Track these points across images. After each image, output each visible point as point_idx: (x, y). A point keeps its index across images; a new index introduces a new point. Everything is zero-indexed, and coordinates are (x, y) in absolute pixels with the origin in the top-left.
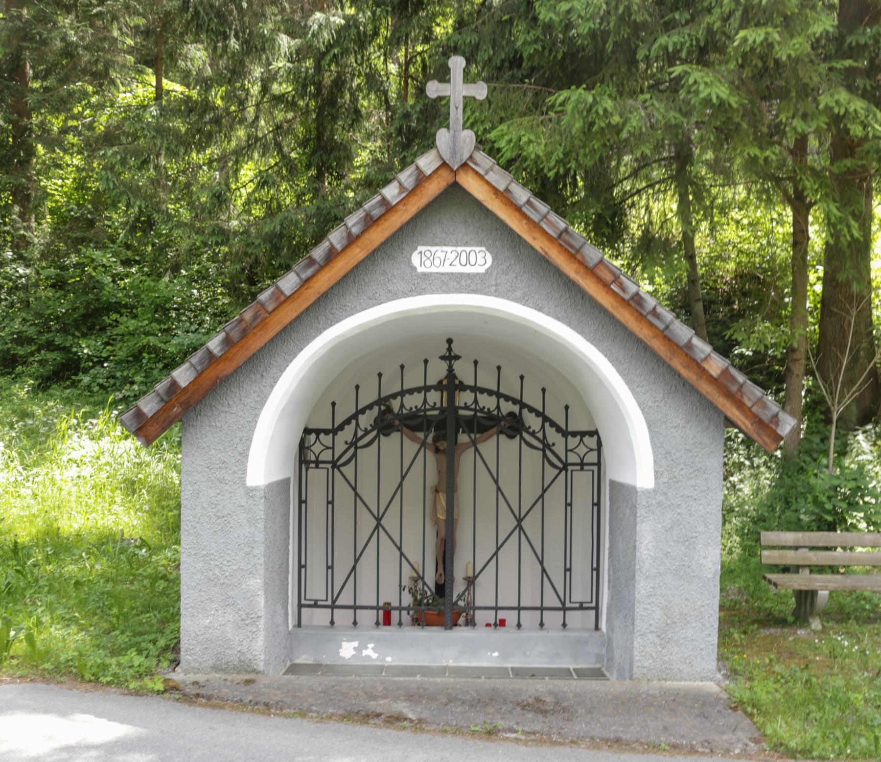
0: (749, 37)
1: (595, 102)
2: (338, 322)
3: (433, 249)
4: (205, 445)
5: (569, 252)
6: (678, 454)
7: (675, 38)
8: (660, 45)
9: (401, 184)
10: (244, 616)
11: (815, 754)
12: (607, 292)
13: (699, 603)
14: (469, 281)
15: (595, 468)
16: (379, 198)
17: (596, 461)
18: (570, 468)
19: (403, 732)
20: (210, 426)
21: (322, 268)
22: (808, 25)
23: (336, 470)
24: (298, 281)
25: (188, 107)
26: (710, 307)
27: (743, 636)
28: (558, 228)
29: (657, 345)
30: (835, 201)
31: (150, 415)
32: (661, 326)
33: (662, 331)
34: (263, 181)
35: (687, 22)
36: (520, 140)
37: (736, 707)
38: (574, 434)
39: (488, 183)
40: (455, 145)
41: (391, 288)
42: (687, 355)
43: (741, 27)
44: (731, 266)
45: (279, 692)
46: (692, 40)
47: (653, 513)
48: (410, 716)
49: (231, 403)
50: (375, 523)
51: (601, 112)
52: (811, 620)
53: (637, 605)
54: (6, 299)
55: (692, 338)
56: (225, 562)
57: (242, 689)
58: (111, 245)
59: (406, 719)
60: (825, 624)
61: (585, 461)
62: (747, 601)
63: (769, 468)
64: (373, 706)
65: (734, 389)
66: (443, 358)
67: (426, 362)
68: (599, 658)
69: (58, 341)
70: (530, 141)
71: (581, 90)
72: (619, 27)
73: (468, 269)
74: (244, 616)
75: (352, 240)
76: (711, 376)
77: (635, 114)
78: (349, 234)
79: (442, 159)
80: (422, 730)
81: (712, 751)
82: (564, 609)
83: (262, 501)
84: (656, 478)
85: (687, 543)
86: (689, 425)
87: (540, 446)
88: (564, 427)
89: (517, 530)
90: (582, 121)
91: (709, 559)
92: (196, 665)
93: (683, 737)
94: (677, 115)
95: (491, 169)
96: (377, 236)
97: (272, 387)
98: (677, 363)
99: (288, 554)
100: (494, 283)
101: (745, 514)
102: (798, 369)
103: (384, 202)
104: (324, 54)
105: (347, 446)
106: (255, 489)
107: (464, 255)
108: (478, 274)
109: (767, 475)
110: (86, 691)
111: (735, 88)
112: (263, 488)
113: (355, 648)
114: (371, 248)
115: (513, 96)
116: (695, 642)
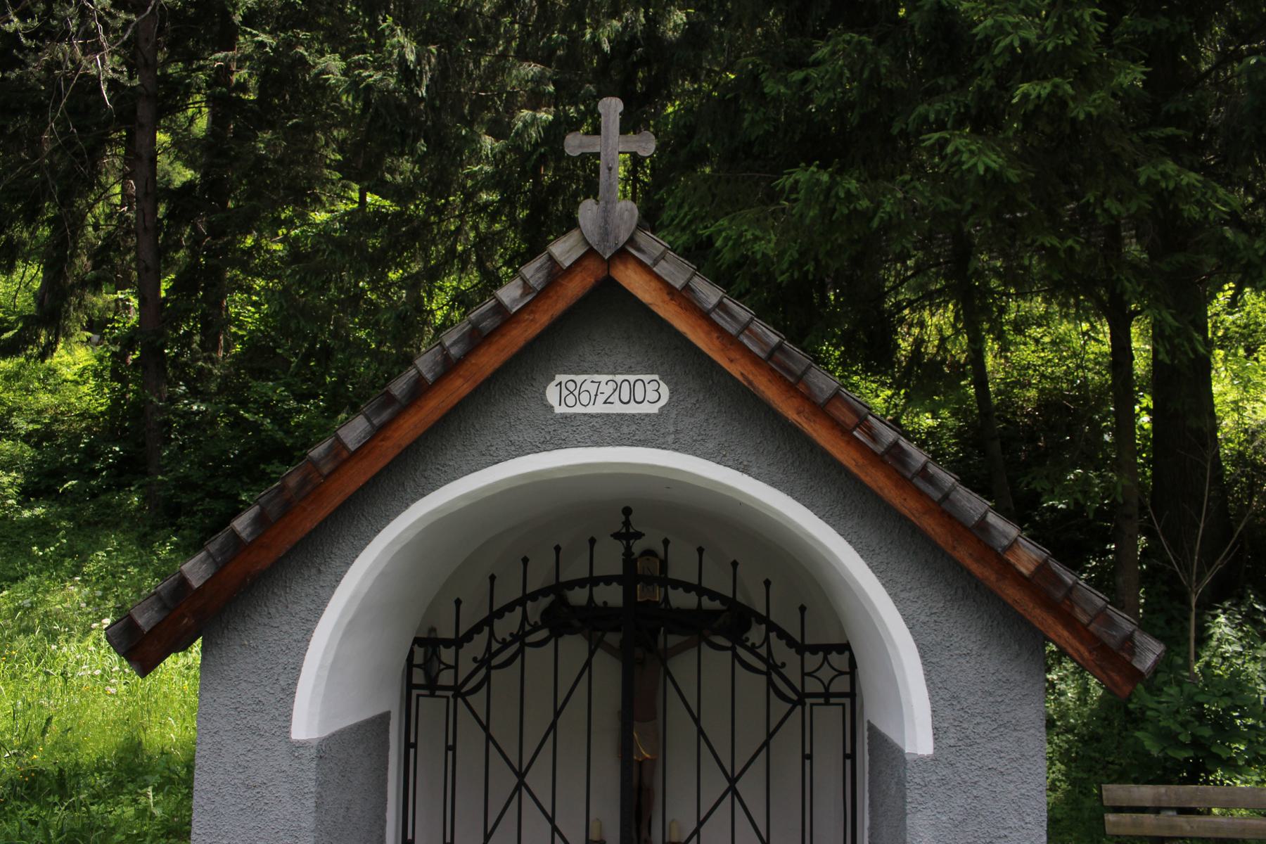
0: (1032, 91)
1: (833, 184)
2: (433, 490)
3: (579, 379)
4: (232, 674)
5: (786, 380)
6: (971, 700)
7: (938, 106)
9: (525, 282)
12: (848, 443)
14: (634, 427)
15: (847, 701)
17: (848, 689)
18: (808, 701)
23: (460, 700)
24: (369, 428)
28: (767, 344)
29: (930, 524)
30: (1168, 307)
31: (147, 630)
32: (937, 495)
33: (939, 503)
35: (954, 89)
36: (741, 235)
38: (814, 649)
39: (658, 277)
40: (606, 222)
41: (514, 438)
42: (979, 541)
44: (1032, 393)
46: (959, 108)
47: (932, 796)
49: (273, 611)
51: (842, 195)
55: (986, 513)
58: (283, 376)
65: (1059, 594)
66: (617, 536)
67: (592, 541)
71: (813, 169)
73: (632, 409)
75: (449, 367)
76: (1021, 574)
77: (889, 196)
78: (446, 357)
79: (587, 243)
83: (313, 765)
86: (987, 652)
87: (762, 667)
89: (729, 796)
90: (817, 207)
95: (663, 257)
96: (489, 360)
97: (334, 588)
98: (963, 554)
99: (383, 828)
100: (672, 429)
101: (1070, 730)
103: (500, 307)
104: (531, 153)
105: (476, 665)
106: (302, 745)
107: (626, 386)
108: (647, 415)
112: (315, 743)
114: (480, 378)
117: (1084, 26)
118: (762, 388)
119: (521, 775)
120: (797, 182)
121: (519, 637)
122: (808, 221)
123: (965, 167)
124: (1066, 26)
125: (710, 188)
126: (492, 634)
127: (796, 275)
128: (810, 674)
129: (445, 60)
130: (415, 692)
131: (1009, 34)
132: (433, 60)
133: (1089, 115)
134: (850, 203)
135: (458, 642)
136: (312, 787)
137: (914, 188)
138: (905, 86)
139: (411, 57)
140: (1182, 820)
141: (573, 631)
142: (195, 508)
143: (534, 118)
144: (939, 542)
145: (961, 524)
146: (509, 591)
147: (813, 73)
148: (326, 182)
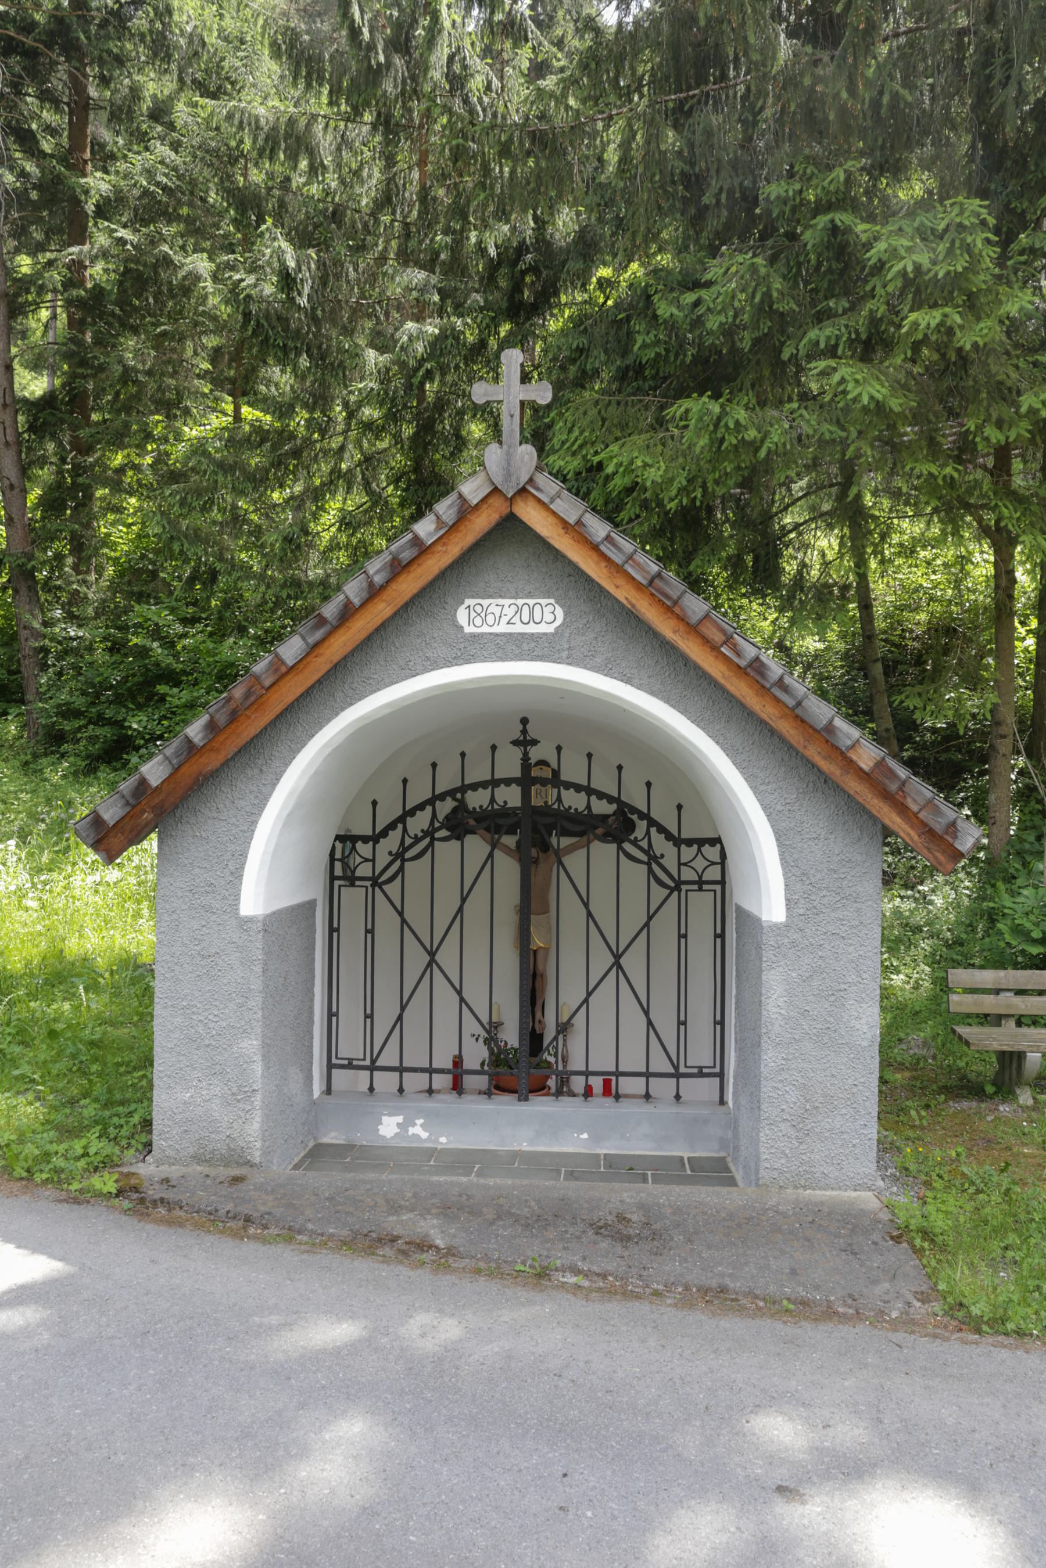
0: (920, 321)
1: (724, 413)
3: (485, 602)
6: (819, 876)
7: (828, 332)
8: (810, 341)
10: (235, 1090)
11: (1010, 1326)
13: (850, 1081)
14: (533, 644)
15: (718, 888)
16: (410, 536)
17: (719, 878)
18: (684, 887)
19: (420, 1271)
20: (194, 836)
21: (335, 629)
22: (1000, 303)
24: (304, 646)
25: (260, 436)
26: (895, 668)
27: (923, 1113)
28: (648, 572)
29: (786, 728)
31: (112, 823)
32: (791, 703)
33: (793, 709)
34: (347, 522)
35: (845, 311)
36: (632, 462)
37: (900, 1236)
38: (689, 842)
39: (554, 513)
40: (509, 464)
43: (911, 310)
44: (923, 617)
45: (271, 1198)
47: (784, 956)
48: (439, 1242)
49: (221, 806)
50: (428, 958)
51: (731, 425)
52: (1018, 1092)
53: (764, 1082)
54: (54, 665)
56: (211, 1017)
57: (223, 1193)
59: (430, 1247)
60: (1039, 1097)
61: (704, 878)
62: (934, 1058)
63: (968, 874)
64: (393, 1224)
65: (893, 787)
66: (515, 743)
67: (494, 748)
68: (723, 1143)
69: (109, 714)
70: (646, 465)
71: (705, 399)
72: (758, 320)
73: (532, 629)
74: (235, 1090)
75: (374, 592)
76: (861, 769)
78: (371, 584)
80: (448, 1268)
81: (858, 1313)
82: (677, 1075)
83: (260, 936)
84: (788, 909)
85: (833, 998)
87: (644, 858)
88: (675, 832)
91: (863, 1021)
92: (172, 1153)
93: (817, 1287)
94: (833, 428)
95: (558, 495)
96: (408, 586)
98: (814, 752)
99: (312, 1000)
100: (566, 646)
102: (1004, 746)
103: (416, 541)
104: (416, 370)
106: (250, 920)
107: (526, 609)
109: (967, 883)
110: (11, 1194)
111: (901, 387)
113: (398, 1125)
115: (632, 411)
116: (845, 1136)
117: (977, 251)
118: (643, 610)
119: (432, 954)
120: (687, 411)
121: (429, 833)
122: (698, 450)
123: (850, 397)
124: (958, 252)
125: (600, 412)
126: (405, 830)
127: (685, 501)
128: (685, 864)
129: (325, 264)
130: (337, 883)
131: (903, 258)
132: (313, 266)
133: (975, 345)
134: (739, 432)
135: (375, 839)
136: (259, 955)
137: (801, 415)
138: (797, 309)
139: (292, 264)
140: (1018, 1000)
141: (473, 832)
142: (79, 735)
143: (421, 332)
144: (793, 742)
145: (811, 727)
146: (419, 793)
147: (704, 293)
148: (198, 394)
